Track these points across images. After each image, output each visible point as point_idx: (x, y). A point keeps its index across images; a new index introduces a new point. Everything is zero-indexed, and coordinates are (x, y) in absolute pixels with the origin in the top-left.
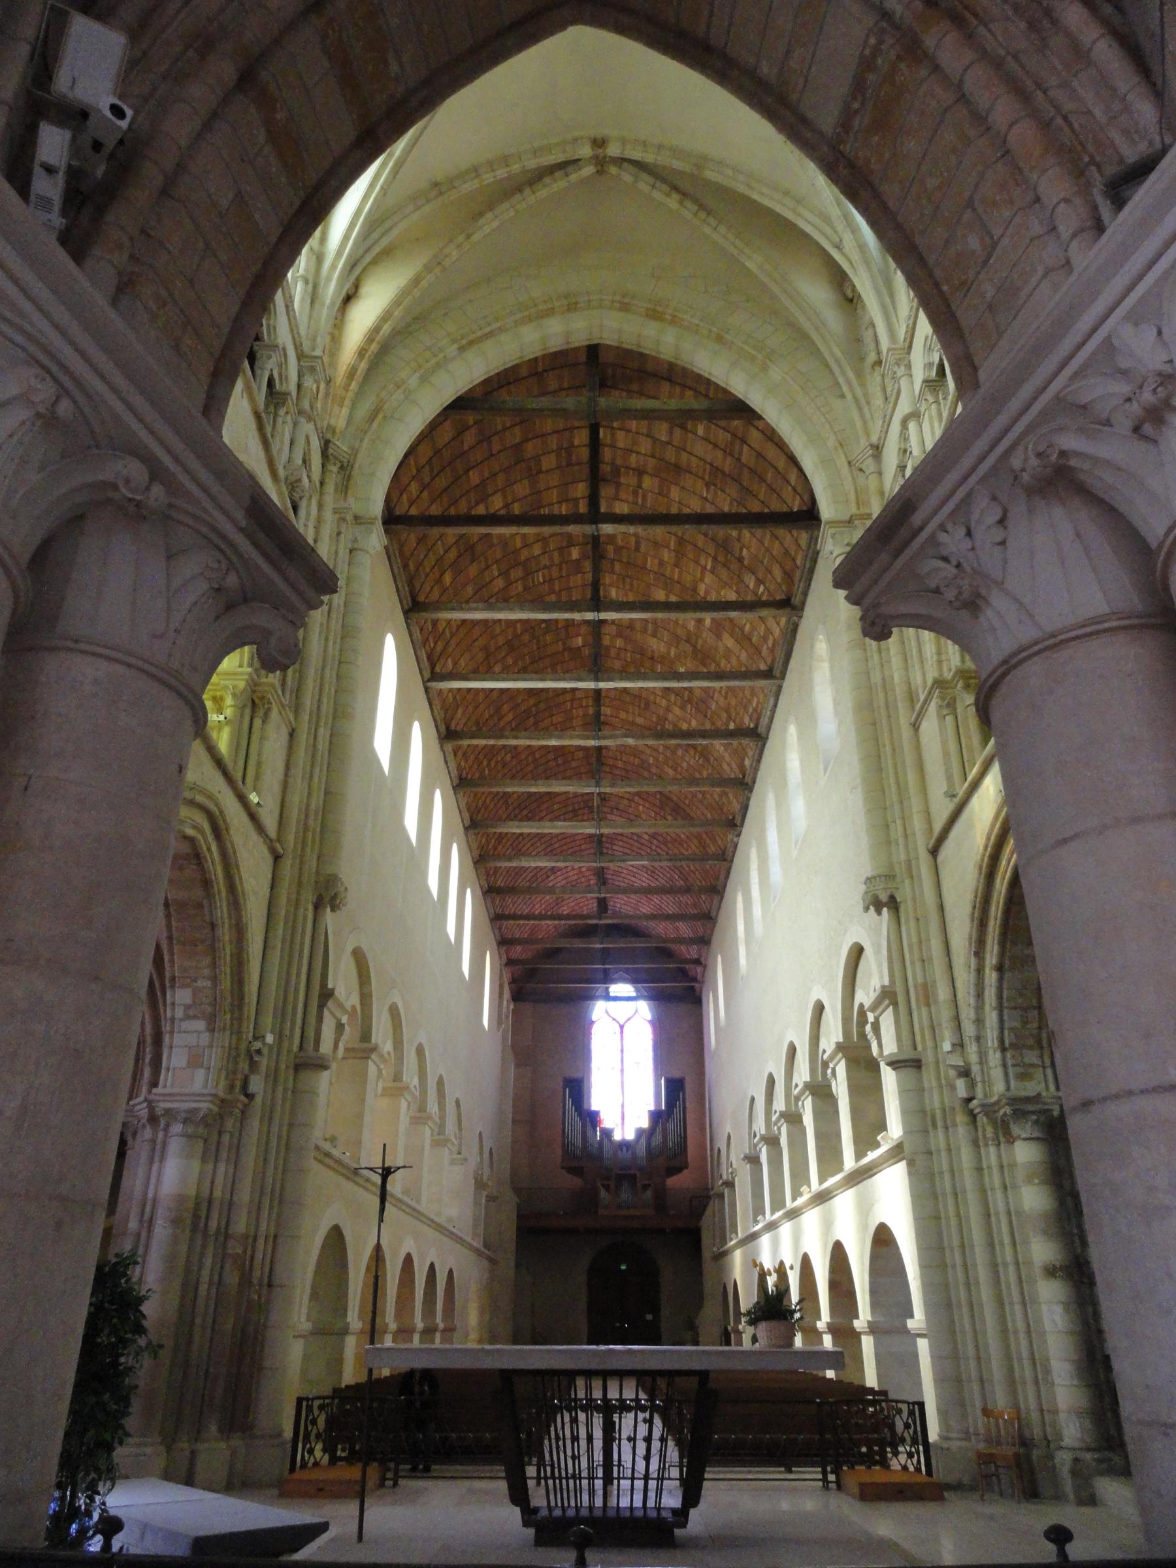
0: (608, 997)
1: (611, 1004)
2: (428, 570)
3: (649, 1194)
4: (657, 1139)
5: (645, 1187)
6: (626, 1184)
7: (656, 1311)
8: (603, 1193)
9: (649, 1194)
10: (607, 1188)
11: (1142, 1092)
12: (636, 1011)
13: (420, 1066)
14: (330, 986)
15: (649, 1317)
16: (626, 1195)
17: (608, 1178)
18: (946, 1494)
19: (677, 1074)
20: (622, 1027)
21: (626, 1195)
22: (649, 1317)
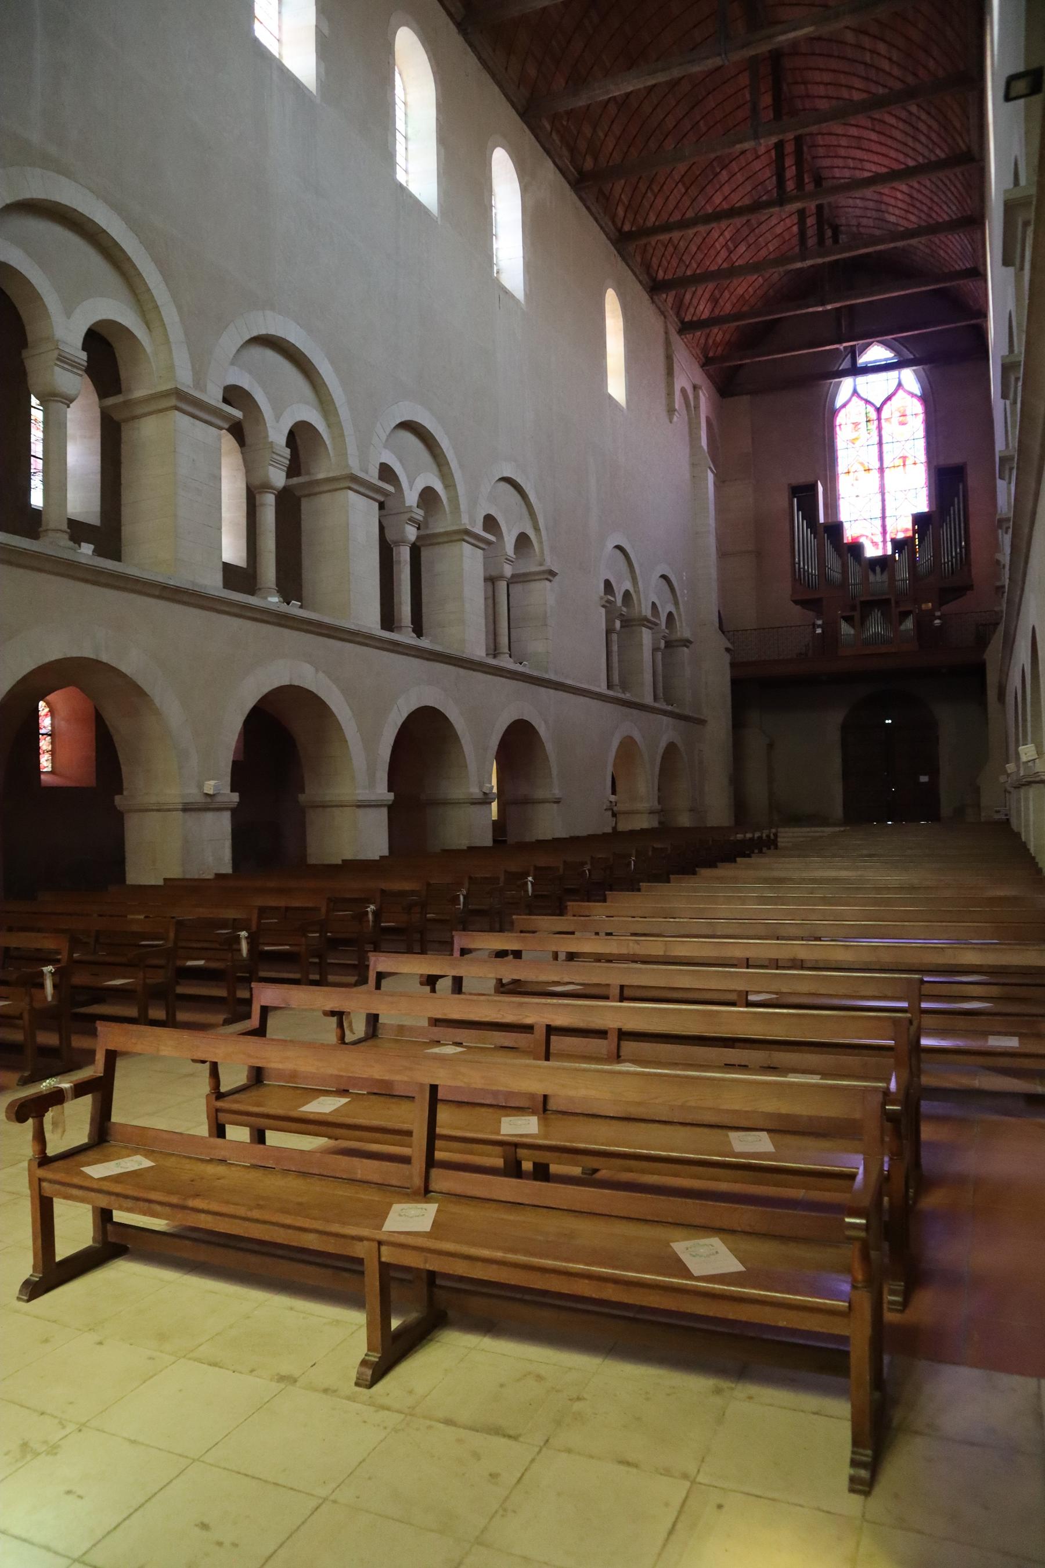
0: (856, 371)
1: (861, 380)
2: (669, 258)
3: (909, 624)
4: (924, 557)
5: (904, 615)
6: (877, 614)
7: (934, 773)
8: (845, 628)
9: (909, 624)
10: (849, 620)
11: (103, 1538)
12: (900, 385)
13: (869, 996)
14: (738, 859)
15: (924, 779)
16: (875, 627)
17: (853, 608)
18: (266, 995)
19: (955, 460)
20: (879, 410)
21: (875, 627)
22: (924, 779)
